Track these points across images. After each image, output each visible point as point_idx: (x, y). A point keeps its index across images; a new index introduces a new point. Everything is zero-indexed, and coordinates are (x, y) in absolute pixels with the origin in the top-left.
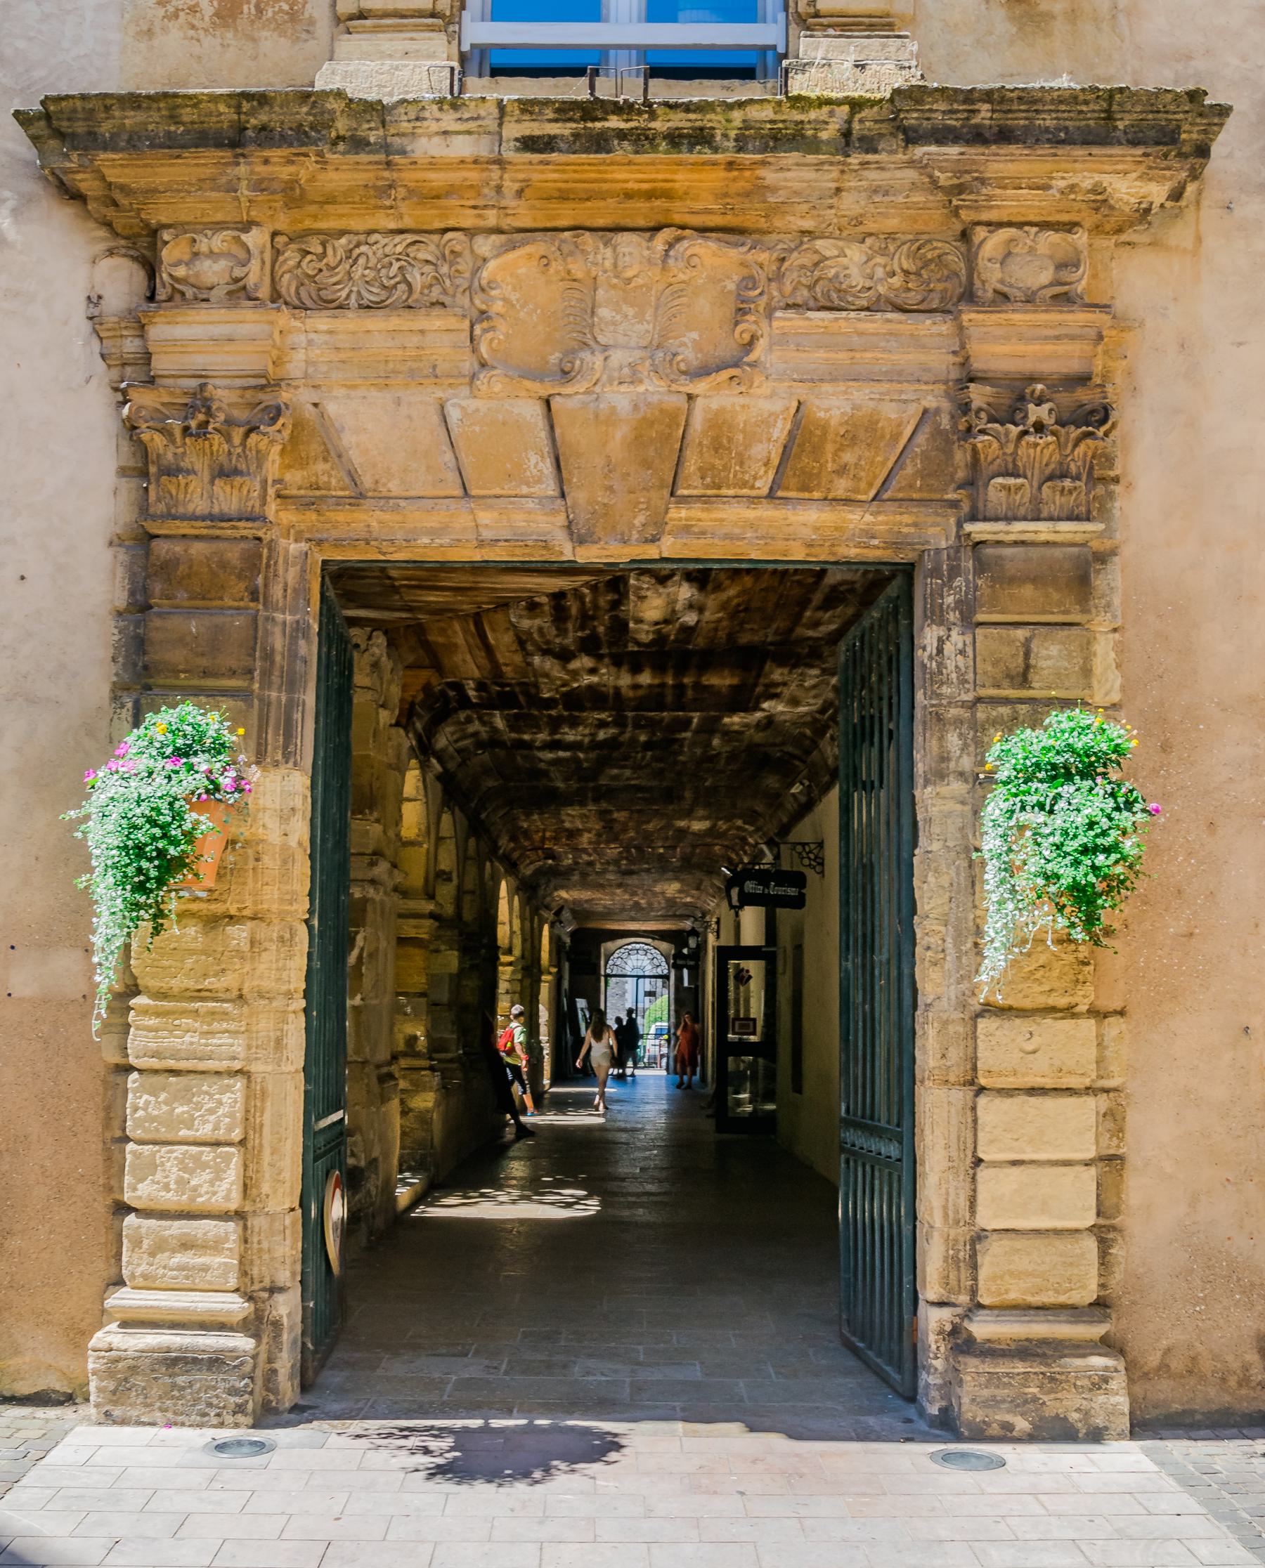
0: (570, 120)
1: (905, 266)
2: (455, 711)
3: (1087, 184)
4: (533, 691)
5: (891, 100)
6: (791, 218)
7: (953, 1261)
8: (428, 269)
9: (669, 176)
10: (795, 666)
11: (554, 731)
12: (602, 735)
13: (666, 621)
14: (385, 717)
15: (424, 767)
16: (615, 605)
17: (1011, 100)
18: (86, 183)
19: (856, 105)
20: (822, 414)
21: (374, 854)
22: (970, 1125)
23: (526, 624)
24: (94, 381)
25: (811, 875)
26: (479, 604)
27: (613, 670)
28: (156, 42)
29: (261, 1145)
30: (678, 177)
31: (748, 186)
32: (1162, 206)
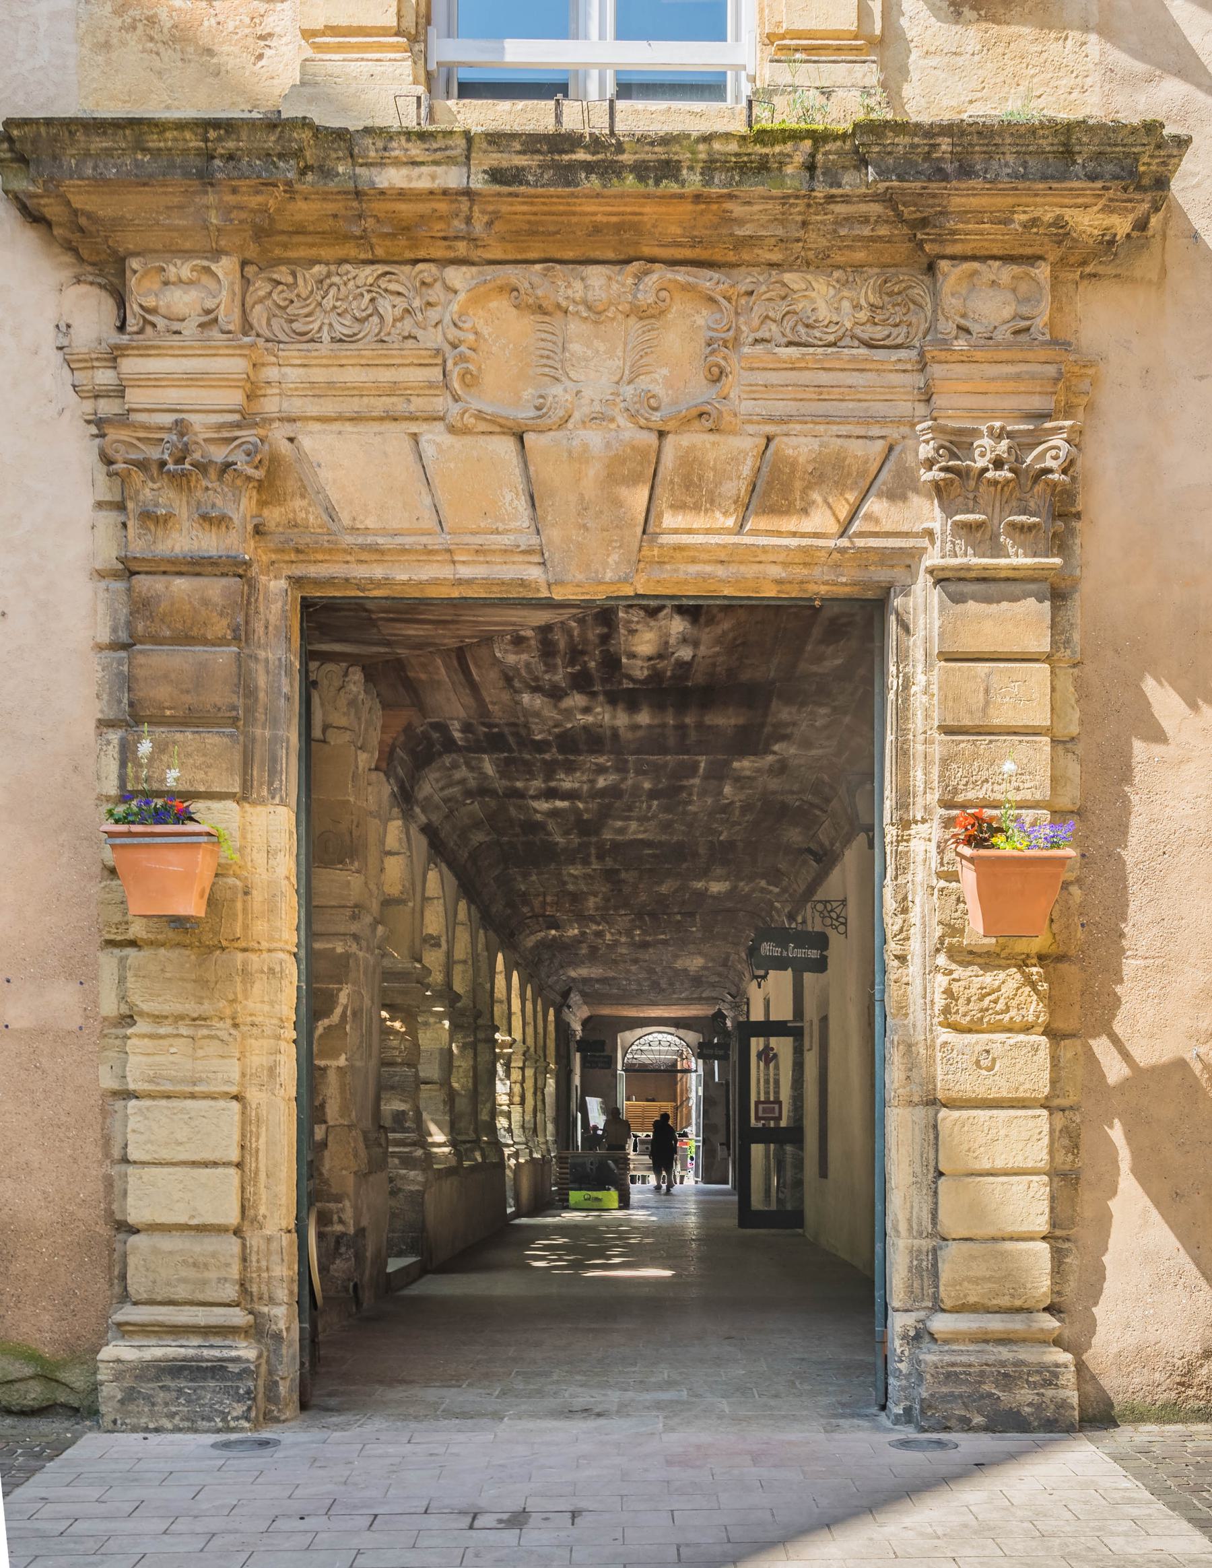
0: (538, 152)
1: (872, 299)
2: (440, 754)
3: (1048, 217)
4: (523, 732)
5: (854, 134)
6: (760, 252)
7: (916, 1271)
8: (398, 300)
9: (637, 209)
10: (803, 704)
11: (549, 777)
12: (601, 782)
13: (660, 656)
14: (364, 760)
15: (407, 815)
16: (605, 639)
17: (971, 134)
18: (52, 209)
19: (819, 138)
20: (790, 452)
21: (356, 906)
22: (932, 1141)
23: (511, 659)
24: (67, 413)
25: (833, 935)
26: (461, 638)
27: (608, 708)
28: (114, 56)
29: (257, 1168)
30: (647, 210)
31: (716, 220)
32: (1128, 236)
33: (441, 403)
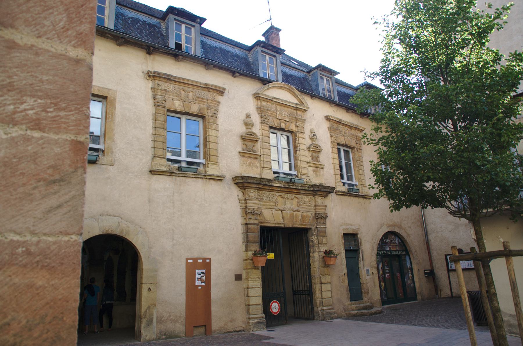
33: (275, 207)
